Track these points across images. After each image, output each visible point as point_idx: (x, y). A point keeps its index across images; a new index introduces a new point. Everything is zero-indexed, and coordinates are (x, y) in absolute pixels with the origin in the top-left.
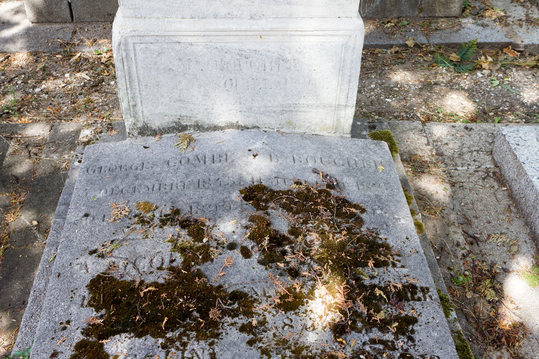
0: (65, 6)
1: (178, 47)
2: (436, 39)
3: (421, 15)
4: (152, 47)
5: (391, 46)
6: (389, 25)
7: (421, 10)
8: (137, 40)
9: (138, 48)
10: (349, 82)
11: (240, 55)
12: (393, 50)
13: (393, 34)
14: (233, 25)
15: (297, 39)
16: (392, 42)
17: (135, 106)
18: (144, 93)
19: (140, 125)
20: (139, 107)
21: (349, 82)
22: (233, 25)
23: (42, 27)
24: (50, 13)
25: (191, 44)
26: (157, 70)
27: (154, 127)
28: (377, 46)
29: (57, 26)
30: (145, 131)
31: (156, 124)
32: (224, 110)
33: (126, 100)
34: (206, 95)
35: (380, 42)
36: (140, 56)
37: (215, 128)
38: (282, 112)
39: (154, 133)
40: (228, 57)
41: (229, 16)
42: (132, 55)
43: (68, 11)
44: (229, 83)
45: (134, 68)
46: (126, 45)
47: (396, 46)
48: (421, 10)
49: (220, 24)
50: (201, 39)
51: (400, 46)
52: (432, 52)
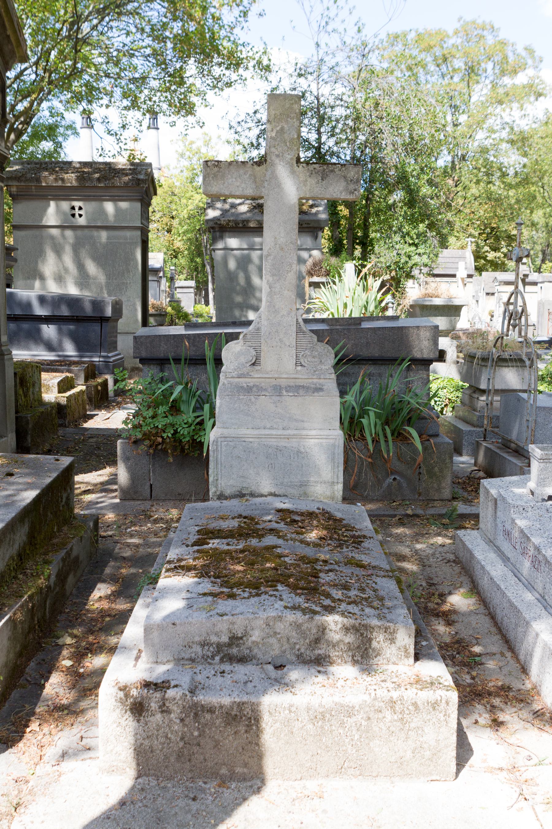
0: (147, 487)
1: (244, 444)
2: (432, 511)
3: (421, 498)
4: (230, 443)
5: (395, 516)
6: (394, 504)
7: (420, 494)
8: (223, 439)
9: (223, 444)
10: (338, 467)
11: (277, 449)
12: (397, 518)
13: (397, 509)
14: (274, 432)
15: (307, 440)
16: (396, 513)
17: (217, 480)
18: (223, 472)
19: (218, 493)
20: (219, 481)
21: (338, 467)
22: (274, 432)
23: (127, 503)
24: (136, 492)
25: (251, 442)
26: (232, 457)
27: (226, 495)
28: (384, 515)
29: (139, 502)
30: (221, 497)
31: (228, 492)
32: (266, 485)
33: (212, 476)
34: (258, 474)
35: (386, 513)
36: (224, 449)
37: (262, 496)
38: (301, 486)
39: (226, 498)
40: (270, 450)
41: (271, 428)
42: (219, 448)
43: (149, 491)
44: (270, 466)
45: (219, 456)
46: (217, 442)
47: (400, 515)
48: (420, 494)
49: (267, 432)
50: (257, 440)
51: (402, 515)
52: (428, 519)
